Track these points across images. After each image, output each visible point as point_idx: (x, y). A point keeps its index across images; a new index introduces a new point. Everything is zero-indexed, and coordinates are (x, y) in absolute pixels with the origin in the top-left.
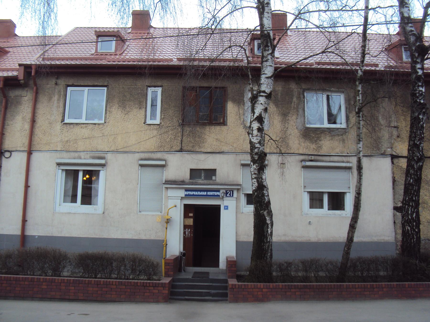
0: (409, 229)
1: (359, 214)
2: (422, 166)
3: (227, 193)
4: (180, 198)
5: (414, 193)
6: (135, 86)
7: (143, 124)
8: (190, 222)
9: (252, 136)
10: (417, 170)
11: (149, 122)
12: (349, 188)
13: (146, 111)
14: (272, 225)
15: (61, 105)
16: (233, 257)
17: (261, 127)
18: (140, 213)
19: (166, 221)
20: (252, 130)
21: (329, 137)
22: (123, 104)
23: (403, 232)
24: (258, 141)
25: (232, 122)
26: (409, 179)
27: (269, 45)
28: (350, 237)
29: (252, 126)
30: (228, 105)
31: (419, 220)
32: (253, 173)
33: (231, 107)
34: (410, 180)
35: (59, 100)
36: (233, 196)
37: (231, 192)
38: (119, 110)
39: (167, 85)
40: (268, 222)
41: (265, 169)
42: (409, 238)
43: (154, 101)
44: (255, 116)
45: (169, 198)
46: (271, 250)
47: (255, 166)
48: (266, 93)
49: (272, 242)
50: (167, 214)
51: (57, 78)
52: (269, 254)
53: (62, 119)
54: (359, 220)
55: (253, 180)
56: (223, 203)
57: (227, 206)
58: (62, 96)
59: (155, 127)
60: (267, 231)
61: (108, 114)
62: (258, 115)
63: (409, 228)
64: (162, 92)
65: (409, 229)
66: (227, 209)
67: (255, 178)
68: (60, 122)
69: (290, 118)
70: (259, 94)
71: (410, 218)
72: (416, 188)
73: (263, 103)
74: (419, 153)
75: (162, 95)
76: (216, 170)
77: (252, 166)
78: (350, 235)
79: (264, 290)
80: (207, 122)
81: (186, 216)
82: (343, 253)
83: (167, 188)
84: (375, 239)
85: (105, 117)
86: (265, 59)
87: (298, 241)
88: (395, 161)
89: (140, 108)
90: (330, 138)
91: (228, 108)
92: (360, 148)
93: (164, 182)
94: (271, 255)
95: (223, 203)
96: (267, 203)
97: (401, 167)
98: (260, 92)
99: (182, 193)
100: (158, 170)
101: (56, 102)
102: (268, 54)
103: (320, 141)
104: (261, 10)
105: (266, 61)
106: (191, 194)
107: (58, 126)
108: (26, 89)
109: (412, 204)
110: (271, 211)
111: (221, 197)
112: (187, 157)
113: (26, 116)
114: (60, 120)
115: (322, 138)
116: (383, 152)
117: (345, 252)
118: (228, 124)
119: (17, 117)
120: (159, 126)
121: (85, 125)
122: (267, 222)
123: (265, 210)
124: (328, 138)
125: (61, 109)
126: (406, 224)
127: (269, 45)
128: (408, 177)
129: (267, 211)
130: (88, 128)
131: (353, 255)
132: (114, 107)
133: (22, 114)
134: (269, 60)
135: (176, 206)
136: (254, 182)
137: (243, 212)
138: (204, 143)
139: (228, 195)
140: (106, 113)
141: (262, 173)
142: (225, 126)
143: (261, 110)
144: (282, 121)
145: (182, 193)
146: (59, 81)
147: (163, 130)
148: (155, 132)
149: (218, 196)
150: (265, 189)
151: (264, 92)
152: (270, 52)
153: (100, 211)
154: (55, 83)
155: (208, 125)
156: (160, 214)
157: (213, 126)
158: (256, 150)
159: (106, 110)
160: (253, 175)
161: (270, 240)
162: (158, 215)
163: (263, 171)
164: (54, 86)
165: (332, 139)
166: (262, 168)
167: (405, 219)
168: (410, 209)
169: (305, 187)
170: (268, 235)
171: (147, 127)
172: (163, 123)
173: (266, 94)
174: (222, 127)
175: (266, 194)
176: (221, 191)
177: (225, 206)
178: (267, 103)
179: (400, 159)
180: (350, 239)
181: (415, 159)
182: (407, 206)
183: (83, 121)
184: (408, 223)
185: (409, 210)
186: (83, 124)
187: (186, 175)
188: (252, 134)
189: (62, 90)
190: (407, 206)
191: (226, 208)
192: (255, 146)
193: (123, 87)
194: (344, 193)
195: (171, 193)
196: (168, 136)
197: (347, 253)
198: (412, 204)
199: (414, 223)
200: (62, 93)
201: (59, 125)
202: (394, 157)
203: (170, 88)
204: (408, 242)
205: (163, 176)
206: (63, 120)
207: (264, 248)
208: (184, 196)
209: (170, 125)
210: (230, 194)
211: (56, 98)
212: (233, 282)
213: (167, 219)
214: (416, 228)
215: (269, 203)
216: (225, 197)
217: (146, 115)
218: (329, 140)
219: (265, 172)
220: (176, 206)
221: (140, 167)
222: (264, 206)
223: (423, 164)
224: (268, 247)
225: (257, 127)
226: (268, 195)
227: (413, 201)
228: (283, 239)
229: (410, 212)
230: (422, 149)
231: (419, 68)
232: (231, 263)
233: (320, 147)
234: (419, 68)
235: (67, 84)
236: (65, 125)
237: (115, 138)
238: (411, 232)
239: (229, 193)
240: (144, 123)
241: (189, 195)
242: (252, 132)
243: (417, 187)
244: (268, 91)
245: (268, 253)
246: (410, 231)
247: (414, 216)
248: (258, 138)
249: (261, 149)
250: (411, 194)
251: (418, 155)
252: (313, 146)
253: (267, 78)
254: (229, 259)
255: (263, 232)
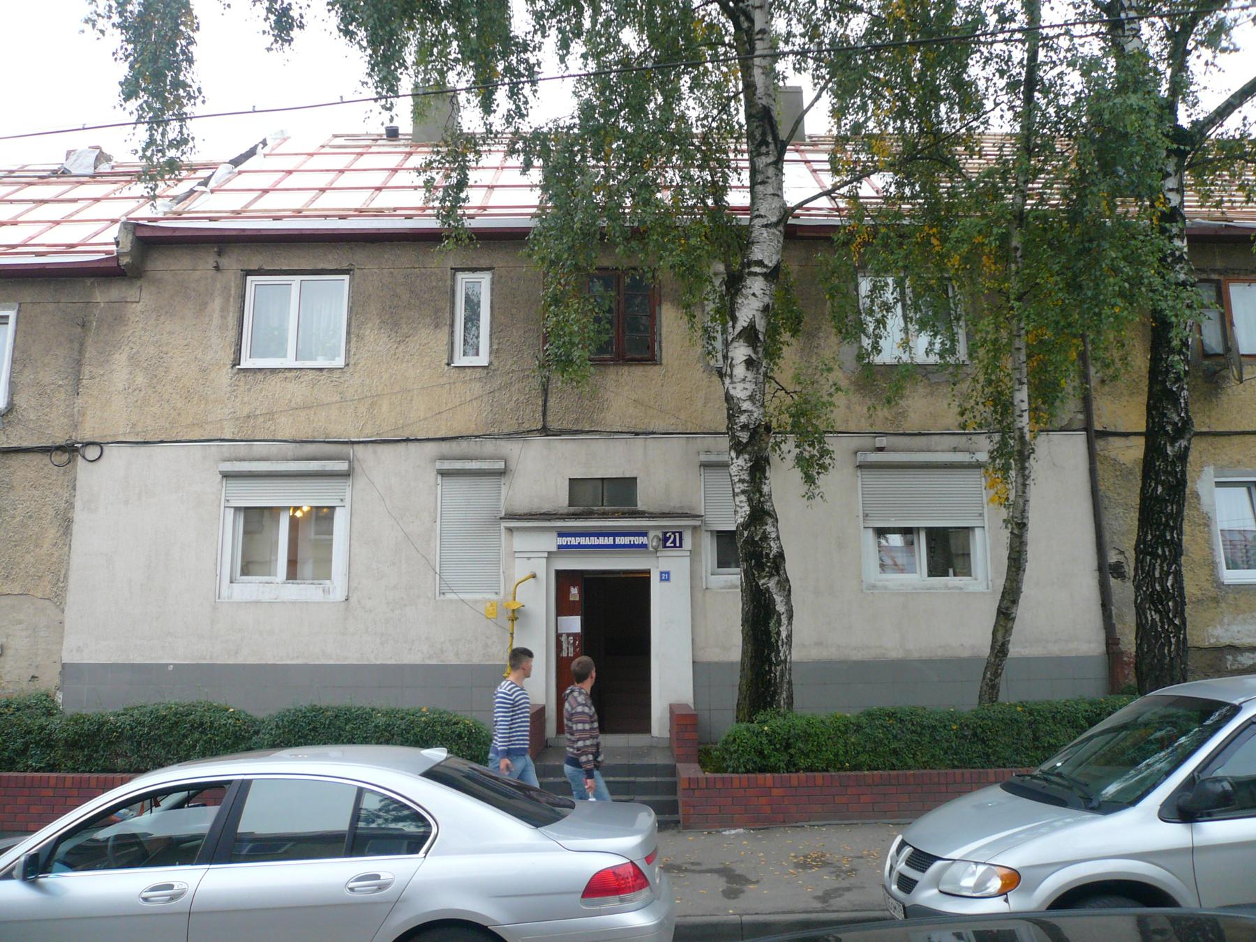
0: (1157, 620)
1: (1022, 580)
2: (1187, 449)
3: (666, 539)
4: (546, 555)
5: (1167, 521)
6: (423, 270)
7: (446, 368)
8: (574, 624)
9: (732, 383)
10: (1173, 461)
11: (460, 360)
12: (981, 515)
13: (452, 333)
14: (790, 618)
15: (232, 320)
16: (687, 705)
17: (754, 356)
18: (442, 596)
19: (510, 614)
20: (732, 366)
21: (925, 387)
22: (392, 317)
23: (1140, 626)
24: (748, 393)
25: (675, 355)
26: (1153, 485)
27: (770, 140)
28: (1000, 644)
29: (730, 354)
30: (663, 312)
31: (1182, 595)
32: (736, 479)
33: (671, 322)
34: (1156, 488)
35: (224, 310)
36: (681, 546)
37: (677, 535)
38: (382, 331)
39: (505, 265)
40: (781, 608)
41: (767, 467)
42: (1156, 643)
43: (472, 306)
44: (739, 328)
45: (517, 555)
46: (790, 683)
47: (741, 462)
48: (766, 266)
49: (791, 662)
50: (511, 597)
51: (219, 254)
52: (784, 695)
53: (235, 359)
54: (1022, 595)
55: (737, 499)
56: (657, 565)
57: (668, 573)
58: (232, 300)
59: (477, 374)
60: (778, 633)
61: (353, 343)
62: (745, 324)
63: (1157, 617)
64: (493, 283)
65: (1157, 620)
66: (668, 580)
67: (743, 492)
68: (229, 366)
69: (822, 342)
70: (747, 271)
71: (1158, 588)
72: (1172, 510)
73: (759, 293)
74: (1179, 415)
75: (492, 290)
76: (636, 478)
77: (735, 461)
78: (1000, 637)
79: (776, 792)
80: (609, 356)
81: (563, 607)
82: (981, 688)
83: (510, 530)
84: (1055, 650)
85: (348, 351)
86: (760, 178)
87: (854, 658)
88: (1100, 444)
89: (436, 327)
90: (928, 390)
91: (663, 319)
92: (1022, 401)
93: (503, 515)
94: (790, 697)
95: (657, 565)
96: (775, 557)
97: (1115, 460)
98: (749, 264)
99: (550, 542)
100: (486, 484)
101: (216, 315)
102: (768, 165)
103: (902, 397)
104: (747, 46)
105: (763, 183)
106: (573, 542)
107: (224, 376)
108: (139, 283)
109: (1164, 552)
110: (787, 580)
111: (651, 549)
112: (562, 447)
113: (138, 352)
114: (229, 363)
115: (906, 392)
116: (1065, 422)
117: (987, 685)
118: (664, 362)
119: (117, 356)
120: (486, 372)
121: (293, 374)
122: (778, 608)
123: (771, 575)
124: (921, 390)
125: (231, 334)
126: (1147, 606)
127: (770, 140)
128: (1152, 479)
129: (776, 578)
130: (302, 380)
131: (1010, 694)
132: (370, 325)
133: (127, 348)
134: (770, 181)
135: (534, 576)
136: (741, 502)
137: (709, 586)
138: (602, 411)
139: (668, 544)
140: (348, 341)
141: (760, 478)
142: (657, 367)
143: (755, 312)
144: (803, 350)
145: (550, 542)
146: (224, 262)
147: (498, 381)
148: (477, 388)
149: (644, 546)
150: (770, 521)
151: (760, 263)
152: (771, 159)
153: (338, 593)
154: (215, 264)
155: (614, 365)
156: (493, 597)
157: (626, 368)
158: (743, 419)
159: (348, 333)
160: (738, 485)
161: (786, 659)
162: (489, 600)
163: (764, 471)
164: (213, 272)
165: (932, 394)
166: (758, 469)
167: (1145, 592)
168: (1157, 567)
169: (866, 516)
170: (780, 643)
171: (454, 372)
172: (496, 364)
173: (765, 270)
174: (648, 368)
175: (773, 535)
176: (652, 534)
177: (661, 573)
178: (768, 292)
179: (1111, 439)
180: (1000, 649)
181: (1167, 432)
182: (1148, 558)
183: (289, 362)
184: (1153, 602)
185: (1154, 569)
186: (290, 369)
187: (561, 499)
188: (731, 376)
189: (233, 284)
190: (1148, 558)
191: (665, 576)
192: (740, 408)
193: (392, 273)
194: (968, 529)
195: (522, 542)
196: (511, 396)
197: (991, 689)
198: (1164, 552)
199: (1170, 604)
200: (233, 292)
201: (227, 373)
202: (1095, 436)
203: (512, 274)
204: (1155, 656)
205: (499, 500)
206: (237, 361)
207: (770, 679)
208: (554, 549)
209: (514, 367)
210: (674, 542)
211: (217, 303)
212: (689, 771)
213: (514, 611)
214: (1175, 617)
215: (781, 556)
216: (661, 548)
217: (452, 344)
218: (925, 397)
219: (767, 474)
220: (534, 576)
221: (439, 477)
222: (769, 567)
223: (1189, 444)
224: (782, 675)
225: (745, 358)
226: (778, 538)
227: (1166, 543)
228: (815, 654)
229: (1157, 574)
230: (1186, 403)
231: (1171, 190)
232: (682, 720)
233: (903, 415)
234: (1171, 190)
235: (246, 268)
236: (242, 374)
237: (373, 404)
238: (1162, 627)
239: (670, 540)
240: (448, 364)
241: (567, 546)
242: (732, 371)
243: (1175, 507)
244: (771, 262)
245: (782, 692)
246: (1159, 624)
247: (1169, 584)
248: (748, 385)
249: (756, 415)
250: (1159, 525)
251: (1177, 419)
252: (883, 413)
253: (766, 226)
254: (677, 712)
255: (768, 633)
